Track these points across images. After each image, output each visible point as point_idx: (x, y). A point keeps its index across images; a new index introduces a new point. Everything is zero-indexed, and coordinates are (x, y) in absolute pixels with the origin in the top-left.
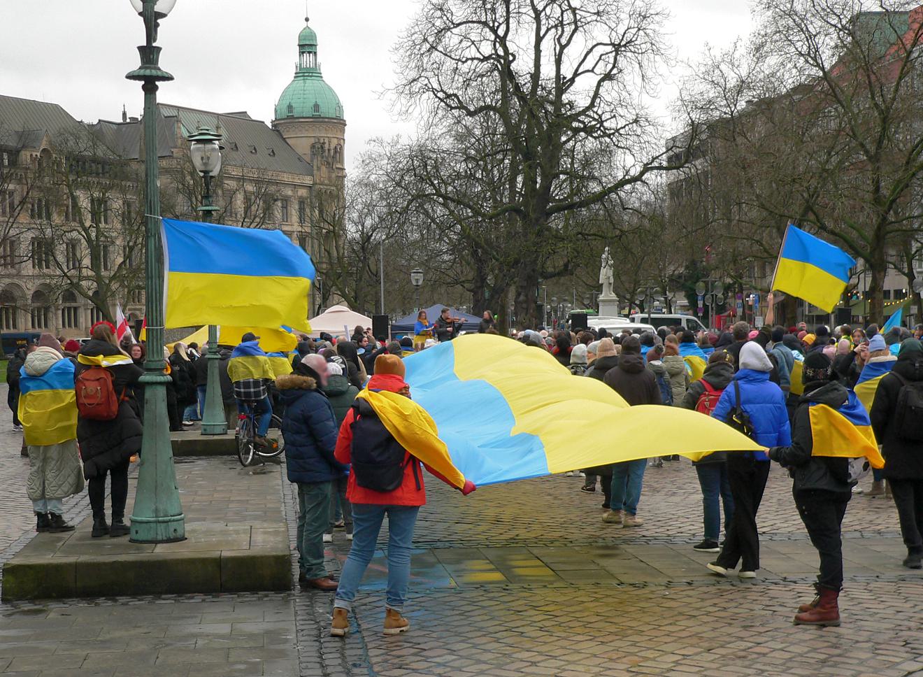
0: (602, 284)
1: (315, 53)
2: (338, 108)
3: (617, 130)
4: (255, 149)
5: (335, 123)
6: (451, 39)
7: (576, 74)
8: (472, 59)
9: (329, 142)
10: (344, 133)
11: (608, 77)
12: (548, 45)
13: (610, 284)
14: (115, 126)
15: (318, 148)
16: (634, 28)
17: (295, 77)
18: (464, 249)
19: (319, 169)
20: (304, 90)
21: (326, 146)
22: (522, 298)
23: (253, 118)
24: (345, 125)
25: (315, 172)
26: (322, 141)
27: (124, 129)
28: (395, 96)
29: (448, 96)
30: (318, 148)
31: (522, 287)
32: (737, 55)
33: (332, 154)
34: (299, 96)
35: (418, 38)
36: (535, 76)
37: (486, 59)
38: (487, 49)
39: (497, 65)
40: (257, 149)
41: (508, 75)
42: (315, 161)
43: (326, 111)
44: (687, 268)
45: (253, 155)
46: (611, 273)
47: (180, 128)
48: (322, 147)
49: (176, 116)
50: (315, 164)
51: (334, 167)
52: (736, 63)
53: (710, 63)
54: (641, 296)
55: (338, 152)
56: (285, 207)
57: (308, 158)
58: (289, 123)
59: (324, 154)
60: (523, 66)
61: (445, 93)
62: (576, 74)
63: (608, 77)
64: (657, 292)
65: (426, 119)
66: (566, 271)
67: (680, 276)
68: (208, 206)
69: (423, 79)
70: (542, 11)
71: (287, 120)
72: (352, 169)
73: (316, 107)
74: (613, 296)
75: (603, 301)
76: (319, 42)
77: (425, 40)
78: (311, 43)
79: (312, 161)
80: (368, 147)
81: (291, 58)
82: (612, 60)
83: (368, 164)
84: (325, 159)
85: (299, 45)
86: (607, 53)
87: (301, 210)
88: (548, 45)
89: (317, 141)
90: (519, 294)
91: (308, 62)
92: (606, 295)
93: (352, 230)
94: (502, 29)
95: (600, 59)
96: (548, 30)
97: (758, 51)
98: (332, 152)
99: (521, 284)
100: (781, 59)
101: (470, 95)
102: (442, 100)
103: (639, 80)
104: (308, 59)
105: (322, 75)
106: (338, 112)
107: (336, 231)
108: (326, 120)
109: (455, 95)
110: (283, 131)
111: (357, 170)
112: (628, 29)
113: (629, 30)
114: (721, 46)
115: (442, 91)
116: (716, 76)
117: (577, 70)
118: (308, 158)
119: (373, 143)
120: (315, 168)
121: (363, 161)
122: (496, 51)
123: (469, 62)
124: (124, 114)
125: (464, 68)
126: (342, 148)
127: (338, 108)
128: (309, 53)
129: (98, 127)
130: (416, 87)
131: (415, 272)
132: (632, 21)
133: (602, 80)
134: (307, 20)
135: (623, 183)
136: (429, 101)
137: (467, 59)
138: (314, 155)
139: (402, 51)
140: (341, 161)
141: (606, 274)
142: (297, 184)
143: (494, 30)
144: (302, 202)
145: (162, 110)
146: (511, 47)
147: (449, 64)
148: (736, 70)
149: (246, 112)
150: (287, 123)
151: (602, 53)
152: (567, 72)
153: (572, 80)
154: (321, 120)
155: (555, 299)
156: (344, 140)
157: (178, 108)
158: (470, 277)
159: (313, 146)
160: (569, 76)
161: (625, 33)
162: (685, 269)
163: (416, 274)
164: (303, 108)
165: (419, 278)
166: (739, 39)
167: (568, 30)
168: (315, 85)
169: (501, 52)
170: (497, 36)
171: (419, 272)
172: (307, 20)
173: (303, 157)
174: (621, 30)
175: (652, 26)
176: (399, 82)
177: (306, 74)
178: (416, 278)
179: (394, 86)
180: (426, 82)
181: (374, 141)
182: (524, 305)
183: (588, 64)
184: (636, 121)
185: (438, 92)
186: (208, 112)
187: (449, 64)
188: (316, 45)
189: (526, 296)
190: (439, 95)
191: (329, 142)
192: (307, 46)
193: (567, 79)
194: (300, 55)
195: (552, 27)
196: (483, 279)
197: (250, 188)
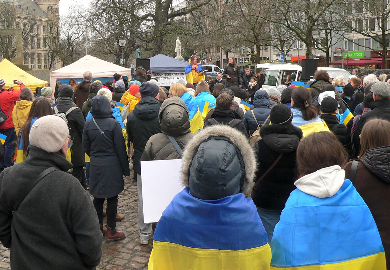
13: (180, 52)
15: (50, 8)
21: (53, 8)
25: (49, 16)
26: (51, 6)
30: (50, 8)
40: (28, 8)
42: (49, 12)
48: (51, 8)
50: (49, 13)
55: (57, 9)
57: (46, 12)
79: (48, 12)
83: (71, 9)
84: (52, 12)
92: (178, 57)
98: (55, 10)
99: (155, 50)
107: (57, 37)
118: (46, 12)
120: (49, 15)
140: (58, 13)
159: (48, 8)
163: (122, 40)
165: (123, 42)
173: (45, 11)
178: (122, 42)
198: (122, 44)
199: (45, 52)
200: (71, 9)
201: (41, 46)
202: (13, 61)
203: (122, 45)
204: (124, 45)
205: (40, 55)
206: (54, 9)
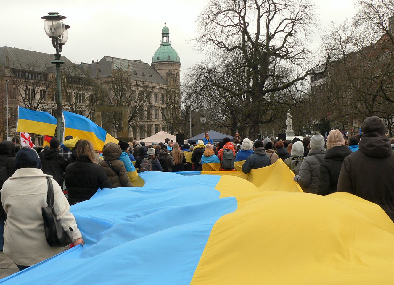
0: (287, 126)
1: (169, 37)
2: (177, 58)
3: (294, 57)
4: (144, 74)
5: (176, 64)
6: (220, 17)
7: (275, 32)
8: (230, 26)
9: (174, 71)
10: (180, 68)
11: (290, 34)
12: (263, 21)
13: (291, 125)
14: (88, 65)
15: (170, 74)
16: (301, 11)
17: (160, 46)
18: (227, 111)
19: (170, 82)
20: (164, 51)
21: (173, 73)
22: (252, 130)
23: (143, 62)
24: (181, 65)
25: (168, 83)
26: (171, 71)
27: (91, 66)
28: (195, 42)
29: (219, 43)
30: (170, 74)
31: (252, 126)
32: (346, 26)
33: (175, 76)
34: (162, 53)
35: (205, 16)
36: (258, 35)
37: (237, 25)
38: (236, 21)
39: (240, 29)
40: (145, 74)
41: (245, 32)
43: (172, 59)
44: (321, 121)
45: (143, 76)
46: (291, 120)
47: (113, 65)
48: (171, 74)
49: (112, 61)
50: (168, 80)
51: (176, 81)
52: (346, 30)
53: (334, 30)
54: (305, 130)
55: (178, 75)
56: (156, 97)
57: (165, 78)
58: (158, 64)
59: (172, 76)
60: (252, 30)
61: (218, 42)
62: (275, 32)
63: (290, 34)
64: (311, 129)
65: (209, 53)
66: (271, 121)
67: (317, 125)
68: (57, 60)
69: (208, 35)
70: (260, 6)
71: (157, 63)
72: (183, 80)
73: (169, 57)
74: (292, 131)
75: (287, 133)
76: (170, 32)
77: (209, 18)
78: (167, 32)
80: (188, 71)
81: (159, 39)
82: (291, 26)
85: (162, 34)
86: (289, 23)
87: (163, 98)
88: (263, 21)
89: (169, 71)
90: (251, 129)
91: (166, 40)
92: (289, 130)
93: (183, 106)
94: (243, 11)
95: (286, 26)
96: (263, 14)
97: (356, 23)
98: (175, 75)
100: (367, 26)
101: (229, 42)
102: (217, 45)
103: (304, 36)
104: (166, 39)
105: (171, 45)
106: (177, 60)
108: (173, 63)
109: (222, 42)
110: (156, 67)
111: (183, 80)
112: (299, 12)
113: (299, 13)
114: (338, 23)
115: (216, 40)
116: (337, 36)
117: (276, 30)
119: (190, 69)
120: (168, 81)
121: (186, 77)
122: (240, 21)
123: (228, 27)
124: (93, 61)
125: (226, 30)
126: (179, 74)
127: (177, 58)
128: (166, 36)
129: (81, 65)
130: (205, 39)
131: (202, 117)
132: (301, 8)
133: (287, 35)
134: (165, 23)
135: (296, 80)
136: (211, 45)
137: (227, 26)
138: (168, 76)
139: (198, 22)
140: (179, 79)
141: (289, 121)
142: (158, 87)
143: (239, 13)
144: (163, 95)
145: (106, 59)
146: (246, 20)
147: (219, 28)
148: (345, 33)
149: (141, 60)
150: (157, 64)
151: (287, 23)
152: (272, 31)
153: (274, 35)
154: (171, 63)
155: (266, 132)
156: (180, 71)
157: (113, 58)
158: (230, 123)
159: (167, 73)
160: (273, 33)
161: (297, 14)
162: (320, 122)
163: (203, 118)
164: (164, 58)
166: (347, 20)
167: (272, 13)
168: (169, 49)
169: (242, 22)
170: (240, 16)
171: (204, 117)
172: (165, 23)
173: (164, 77)
174: (296, 13)
175: (310, 11)
176: (197, 37)
177: (165, 45)
178: (203, 119)
179: (195, 38)
180: (209, 37)
181: (191, 68)
182: (253, 134)
183: (281, 28)
184: (303, 51)
185: (215, 41)
186: (123, 59)
187: (219, 28)
188: (169, 34)
189: (254, 129)
190: (216, 42)
191: (174, 71)
192: (165, 33)
193: (272, 34)
194: (162, 37)
195: (265, 13)
196: (236, 124)
197: (140, 89)
198: (203, 121)
199: (163, 124)
200: (188, 77)
201: (159, 118)
202: (120, 134)
203: (203, 122)
204: (205, 122)
205: (158, 127)
206: (174, 75)
